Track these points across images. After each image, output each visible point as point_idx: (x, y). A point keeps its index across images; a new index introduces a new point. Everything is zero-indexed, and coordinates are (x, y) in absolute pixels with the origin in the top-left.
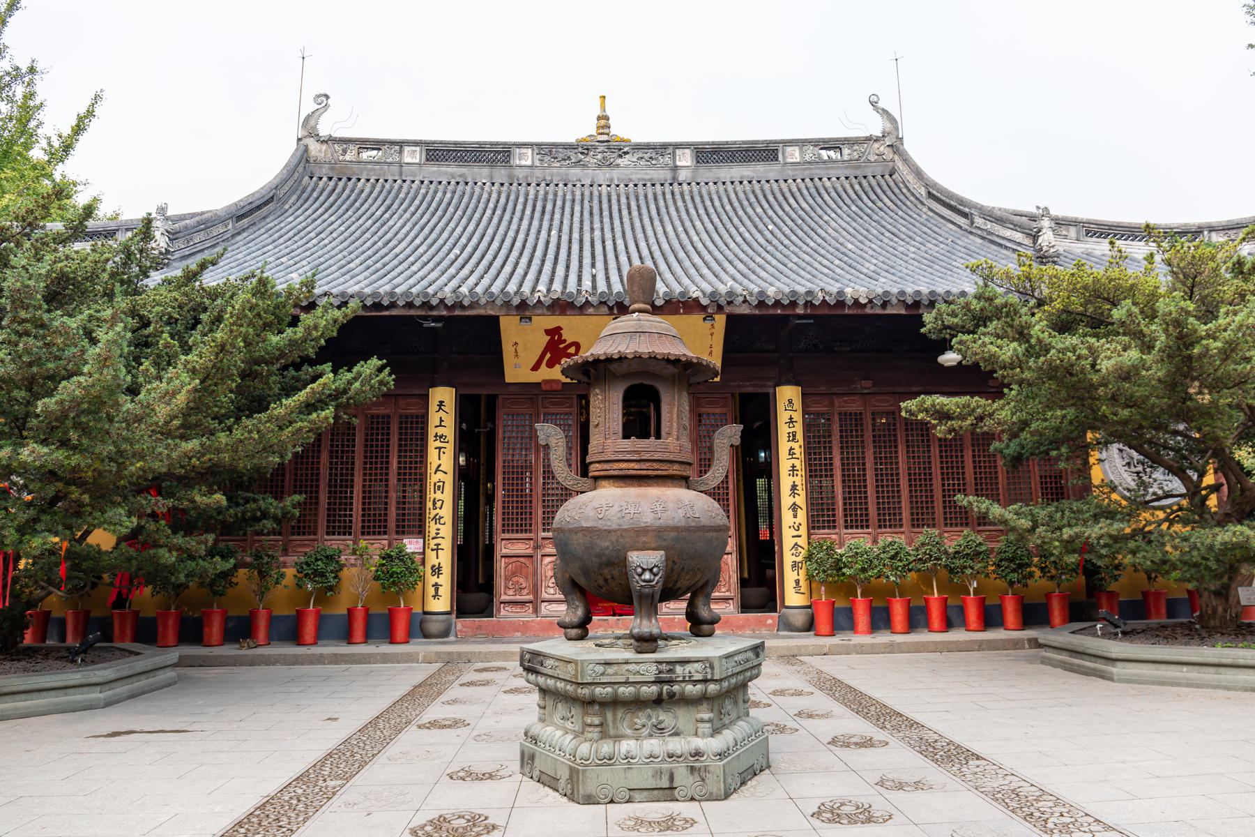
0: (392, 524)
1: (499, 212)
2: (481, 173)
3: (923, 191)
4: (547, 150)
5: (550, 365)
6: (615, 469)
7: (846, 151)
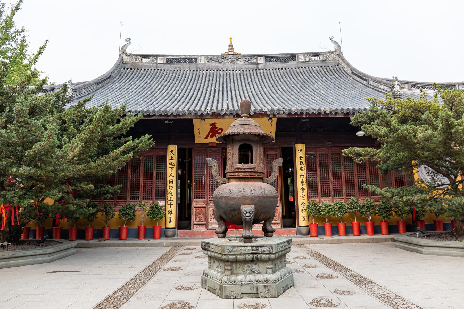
0: (154, 196)
1: (193, 81)
2: (186, 66)
3: (350, 71)
4: (210, 58)
5: (212, 137)
7: (321, 57)
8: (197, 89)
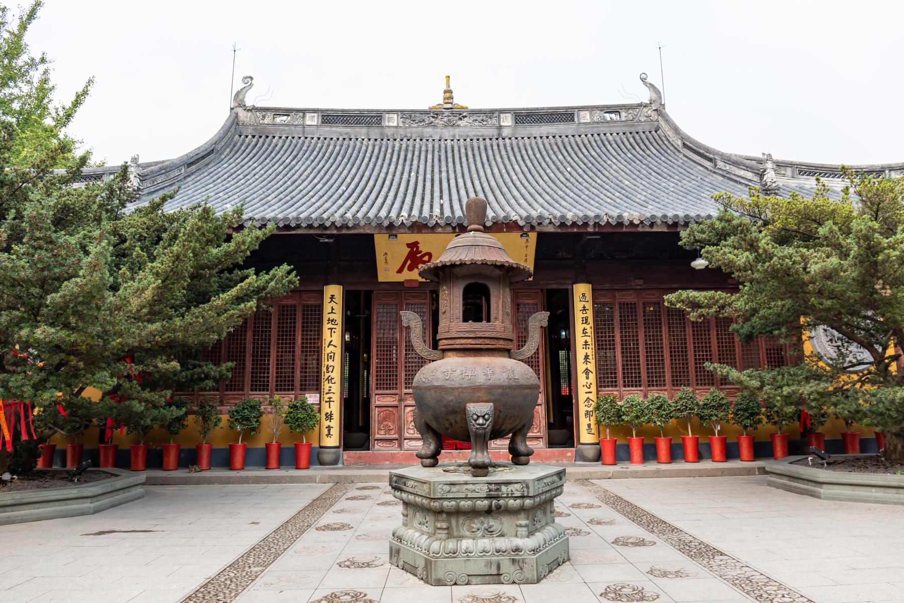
0: (297, 384)
2: (361, 132)
3: (680, 143)
4: (408, 115)
5: (411, 269)
6: (458, 344)
7: (623, 114)
8: (382, 175)
